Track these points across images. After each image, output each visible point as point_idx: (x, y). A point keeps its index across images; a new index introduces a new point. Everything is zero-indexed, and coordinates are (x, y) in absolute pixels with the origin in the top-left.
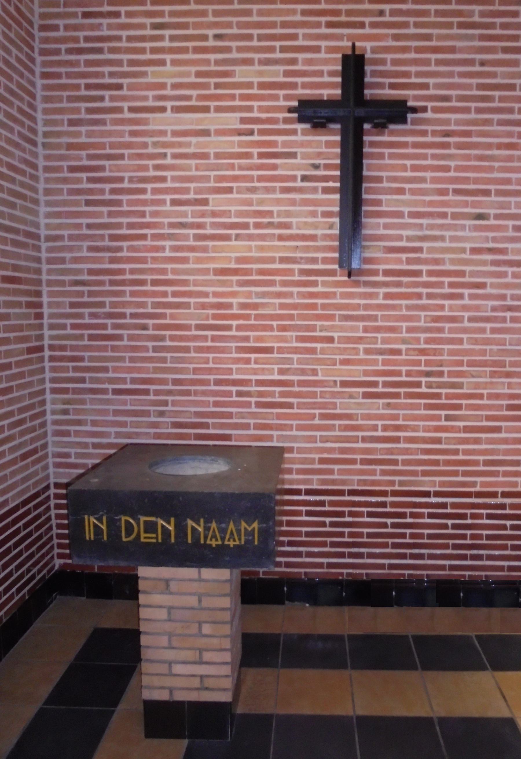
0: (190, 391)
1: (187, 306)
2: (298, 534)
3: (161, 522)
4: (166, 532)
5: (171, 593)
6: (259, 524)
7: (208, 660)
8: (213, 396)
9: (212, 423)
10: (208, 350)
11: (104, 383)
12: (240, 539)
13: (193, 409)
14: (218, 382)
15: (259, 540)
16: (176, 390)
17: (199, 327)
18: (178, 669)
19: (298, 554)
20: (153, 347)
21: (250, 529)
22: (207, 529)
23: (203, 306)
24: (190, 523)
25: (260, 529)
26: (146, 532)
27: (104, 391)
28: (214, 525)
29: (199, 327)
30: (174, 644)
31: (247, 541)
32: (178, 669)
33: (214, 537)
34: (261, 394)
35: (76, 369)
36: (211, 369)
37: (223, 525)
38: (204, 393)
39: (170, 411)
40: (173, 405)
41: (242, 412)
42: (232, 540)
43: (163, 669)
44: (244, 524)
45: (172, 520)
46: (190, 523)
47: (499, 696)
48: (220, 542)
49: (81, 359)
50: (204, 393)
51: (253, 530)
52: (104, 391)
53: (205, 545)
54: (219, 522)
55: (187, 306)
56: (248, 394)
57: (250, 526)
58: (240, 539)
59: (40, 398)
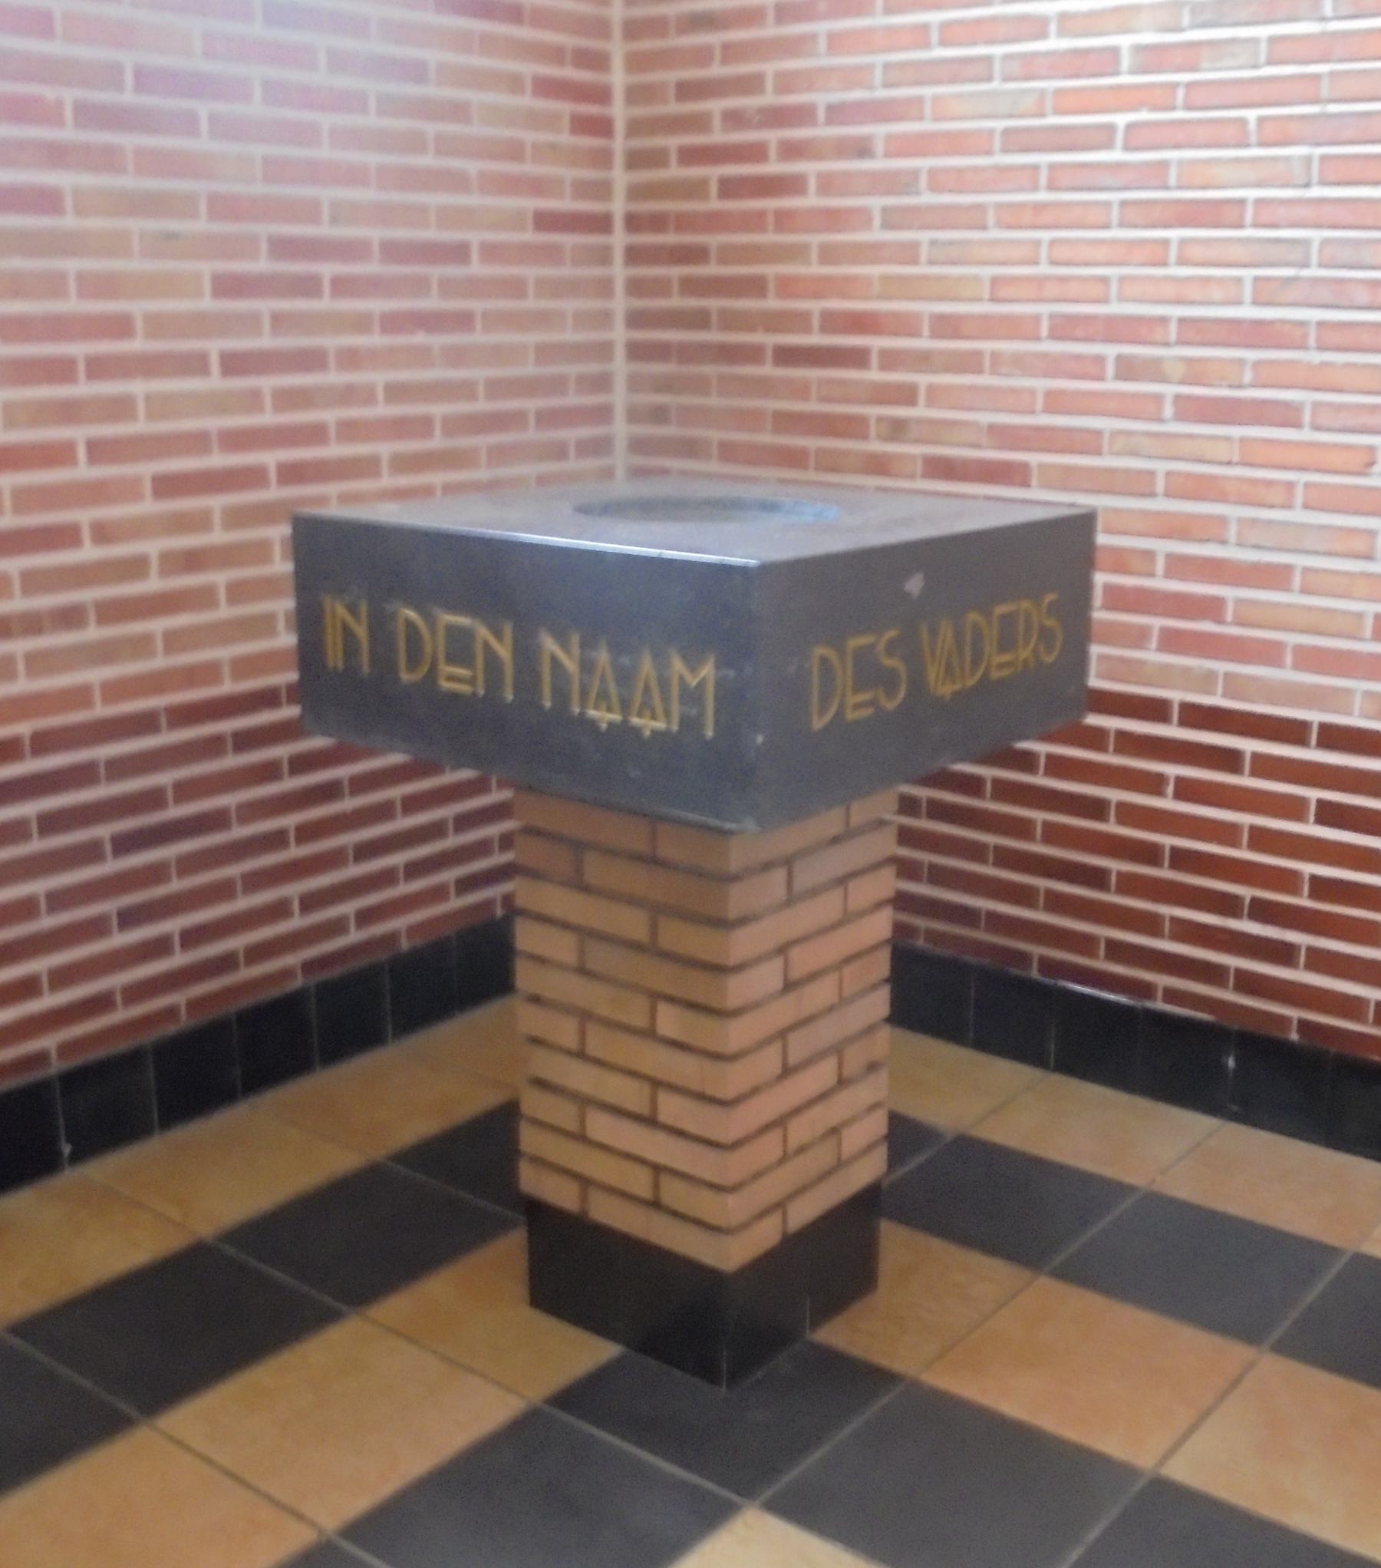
0: (977, 355)
1: (981, 70)
2: (1287, 881)
3: (483, 632)
4: (492, 662)
5: (585, 889)
6: (717, 668)
7: (670, 1121)
8: (1047, 375)
9: (1041, 466)
10: (1039, 216)
11: (752, 328)
12: (667, 714)
13: (986, 418)
14: (1064, 328)
15: (717, 722)
16: (942, 353)
17: (1015, 140)
18: (601, 1126)
19: (1284, 954)
20: (886, 211)
21: (694, 683)
22: (587, 666)
23: (1029, 67)
24: (549, 644)
25: (719, 685)
26: (451, 659)
27: (753, 354)
28: (603, 657)
29: (1015, 140)
30: (594, 1048)
31: (685, 722)
32: (601, 1126)
33: (603, 696)
34: (1195, 373)
35: (690, 286)
36: (1041, 281)
37: (625, 660)
38: (1022, 364)
39: (920, 421)
40: (931, 402)
41: (1129, 433)
42: (647, 713)
43: (564, 1114)
44: (678, 666)
45: (508, 629)
46: (549, 644)
47: (706, 1193)
48: (616, 717)
49: (698, 255)
50: (1022, 364)
51: (701, 685)
52: (753, 354)
53: (582, 719)
54: (616, 649)
55: (981, 70)
56: (1153, 370)
57: (693, 670)
58: (667, 714)
59: (593, 368)
